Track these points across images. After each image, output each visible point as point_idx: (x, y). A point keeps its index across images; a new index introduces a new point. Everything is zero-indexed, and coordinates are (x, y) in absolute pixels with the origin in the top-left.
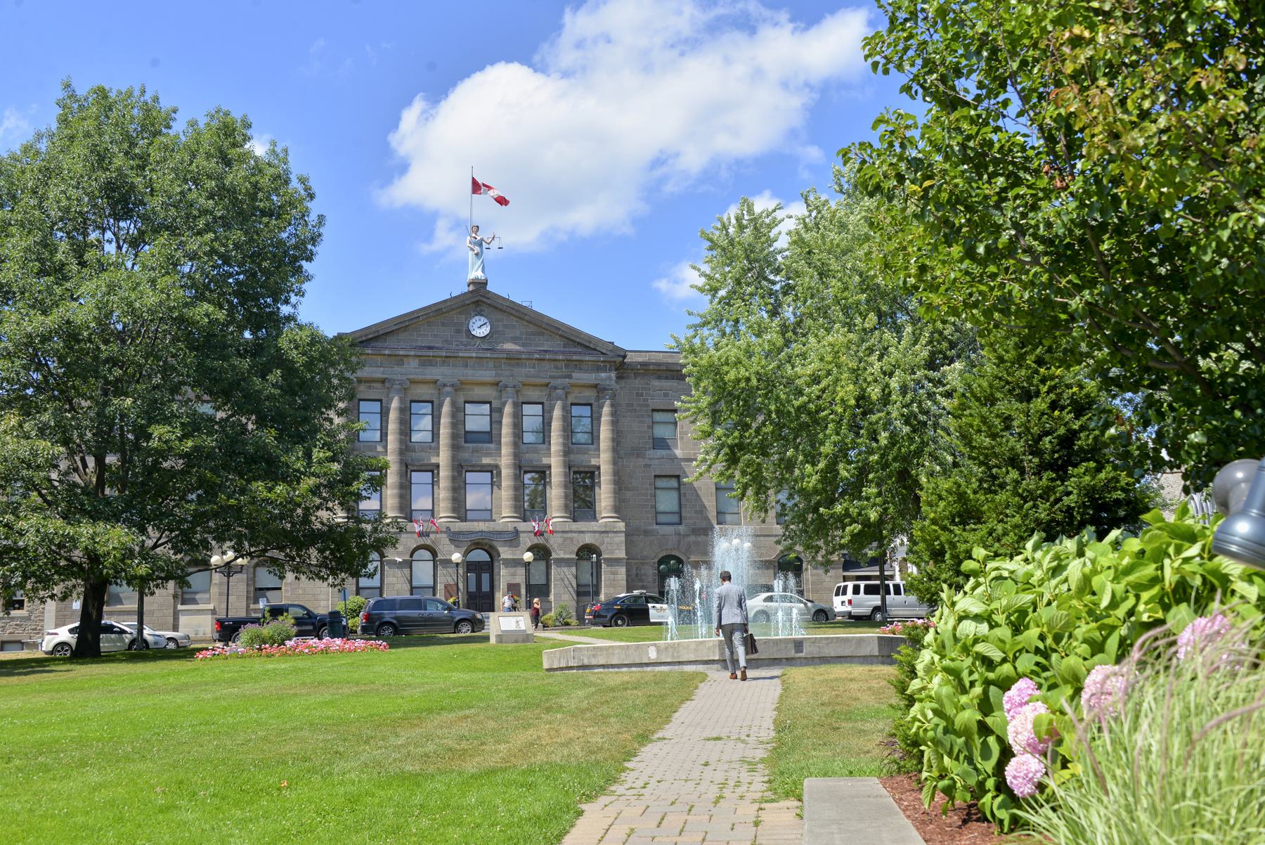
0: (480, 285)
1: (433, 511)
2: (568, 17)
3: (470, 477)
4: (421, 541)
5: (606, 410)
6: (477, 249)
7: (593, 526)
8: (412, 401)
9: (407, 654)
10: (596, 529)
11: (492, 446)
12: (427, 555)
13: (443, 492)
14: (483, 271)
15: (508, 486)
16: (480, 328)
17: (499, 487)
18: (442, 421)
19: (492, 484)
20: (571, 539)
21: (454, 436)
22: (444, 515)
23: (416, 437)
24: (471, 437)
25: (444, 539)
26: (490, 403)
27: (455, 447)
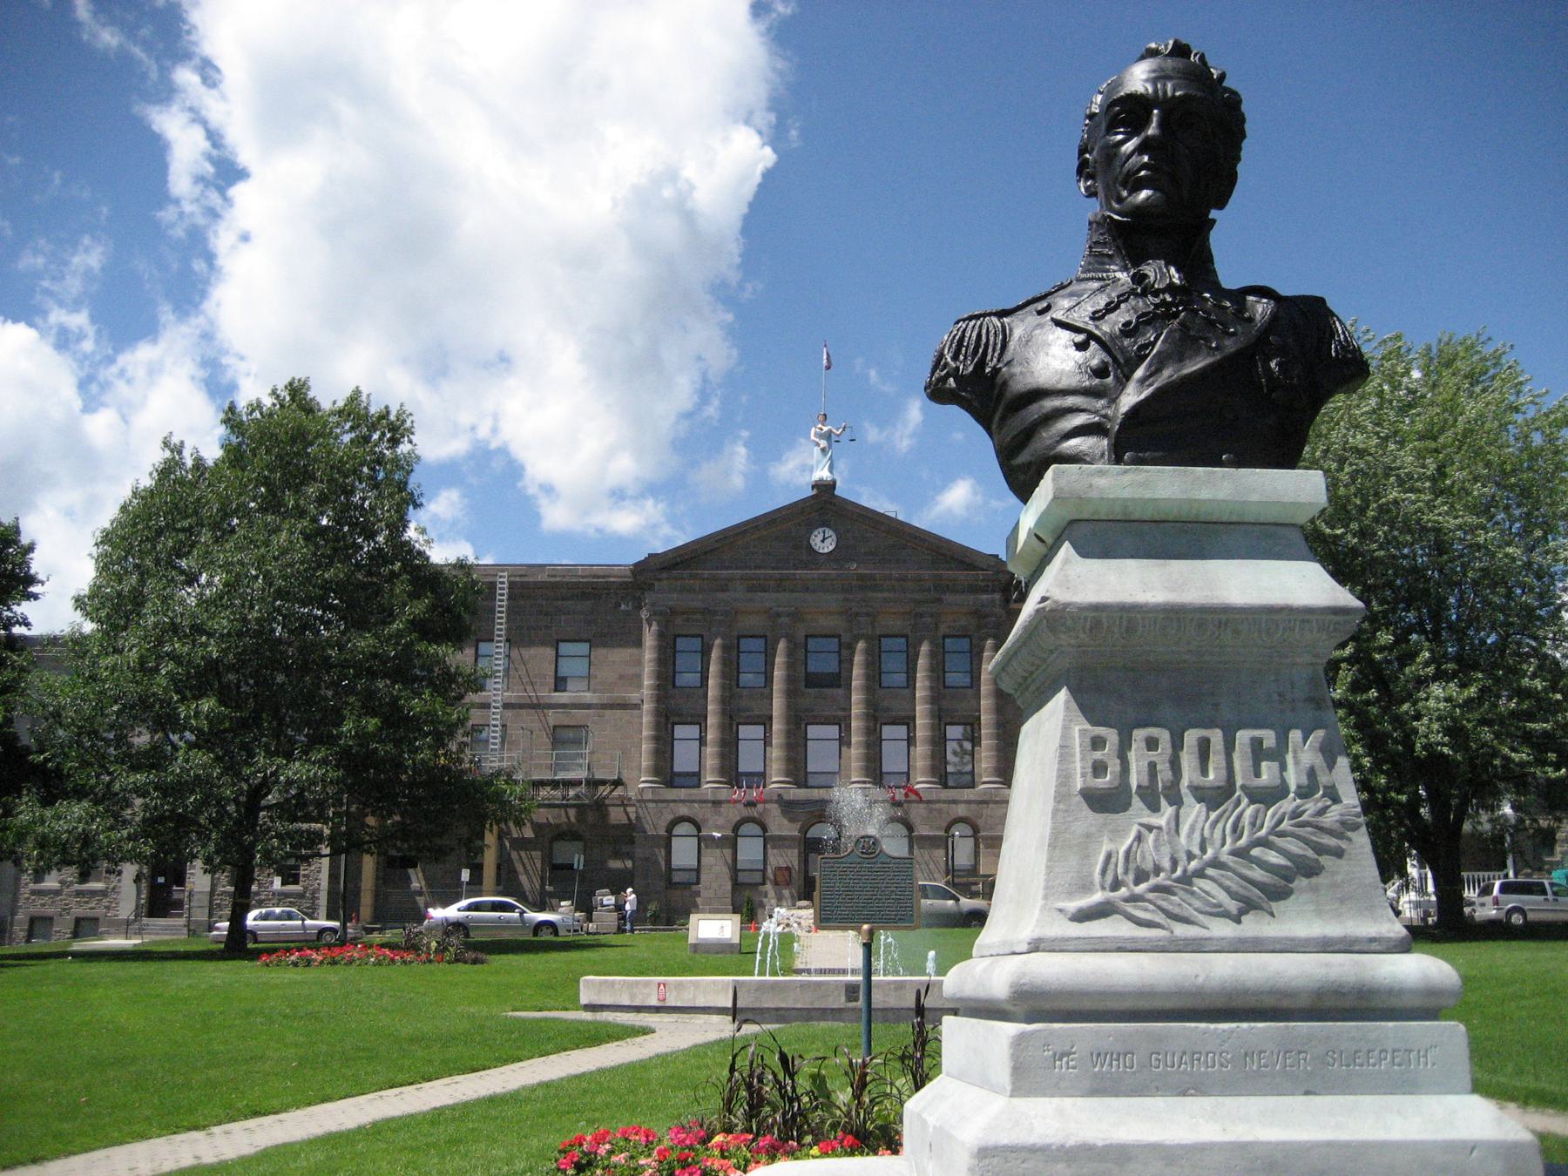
0: (825, 489)
1: (908, 774)
2: (768, 156)
3: (813, 731)
4: (747, 812)
5: (925, 648)
6: (823, 443)
7: (967, 794)
8: (944, 637)
9: (1547, 954)
10: (972, 797)
11: (840, 691)
12: (757, 830)
13: (921, 750)
14: (831, 469)
15: (858, 743)
16: (824, 542)
17: (849, 745)
18: (778, 660)
19: (840, 739)
20: (940, 811)
21: (790, 679)
22: (776, 780)
23: (887, 680)
24: (813, 681)
25: (775, 810)
26: (839, 636)
27: (791, 693)
